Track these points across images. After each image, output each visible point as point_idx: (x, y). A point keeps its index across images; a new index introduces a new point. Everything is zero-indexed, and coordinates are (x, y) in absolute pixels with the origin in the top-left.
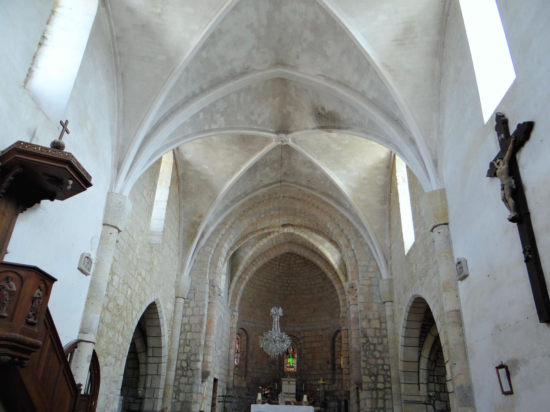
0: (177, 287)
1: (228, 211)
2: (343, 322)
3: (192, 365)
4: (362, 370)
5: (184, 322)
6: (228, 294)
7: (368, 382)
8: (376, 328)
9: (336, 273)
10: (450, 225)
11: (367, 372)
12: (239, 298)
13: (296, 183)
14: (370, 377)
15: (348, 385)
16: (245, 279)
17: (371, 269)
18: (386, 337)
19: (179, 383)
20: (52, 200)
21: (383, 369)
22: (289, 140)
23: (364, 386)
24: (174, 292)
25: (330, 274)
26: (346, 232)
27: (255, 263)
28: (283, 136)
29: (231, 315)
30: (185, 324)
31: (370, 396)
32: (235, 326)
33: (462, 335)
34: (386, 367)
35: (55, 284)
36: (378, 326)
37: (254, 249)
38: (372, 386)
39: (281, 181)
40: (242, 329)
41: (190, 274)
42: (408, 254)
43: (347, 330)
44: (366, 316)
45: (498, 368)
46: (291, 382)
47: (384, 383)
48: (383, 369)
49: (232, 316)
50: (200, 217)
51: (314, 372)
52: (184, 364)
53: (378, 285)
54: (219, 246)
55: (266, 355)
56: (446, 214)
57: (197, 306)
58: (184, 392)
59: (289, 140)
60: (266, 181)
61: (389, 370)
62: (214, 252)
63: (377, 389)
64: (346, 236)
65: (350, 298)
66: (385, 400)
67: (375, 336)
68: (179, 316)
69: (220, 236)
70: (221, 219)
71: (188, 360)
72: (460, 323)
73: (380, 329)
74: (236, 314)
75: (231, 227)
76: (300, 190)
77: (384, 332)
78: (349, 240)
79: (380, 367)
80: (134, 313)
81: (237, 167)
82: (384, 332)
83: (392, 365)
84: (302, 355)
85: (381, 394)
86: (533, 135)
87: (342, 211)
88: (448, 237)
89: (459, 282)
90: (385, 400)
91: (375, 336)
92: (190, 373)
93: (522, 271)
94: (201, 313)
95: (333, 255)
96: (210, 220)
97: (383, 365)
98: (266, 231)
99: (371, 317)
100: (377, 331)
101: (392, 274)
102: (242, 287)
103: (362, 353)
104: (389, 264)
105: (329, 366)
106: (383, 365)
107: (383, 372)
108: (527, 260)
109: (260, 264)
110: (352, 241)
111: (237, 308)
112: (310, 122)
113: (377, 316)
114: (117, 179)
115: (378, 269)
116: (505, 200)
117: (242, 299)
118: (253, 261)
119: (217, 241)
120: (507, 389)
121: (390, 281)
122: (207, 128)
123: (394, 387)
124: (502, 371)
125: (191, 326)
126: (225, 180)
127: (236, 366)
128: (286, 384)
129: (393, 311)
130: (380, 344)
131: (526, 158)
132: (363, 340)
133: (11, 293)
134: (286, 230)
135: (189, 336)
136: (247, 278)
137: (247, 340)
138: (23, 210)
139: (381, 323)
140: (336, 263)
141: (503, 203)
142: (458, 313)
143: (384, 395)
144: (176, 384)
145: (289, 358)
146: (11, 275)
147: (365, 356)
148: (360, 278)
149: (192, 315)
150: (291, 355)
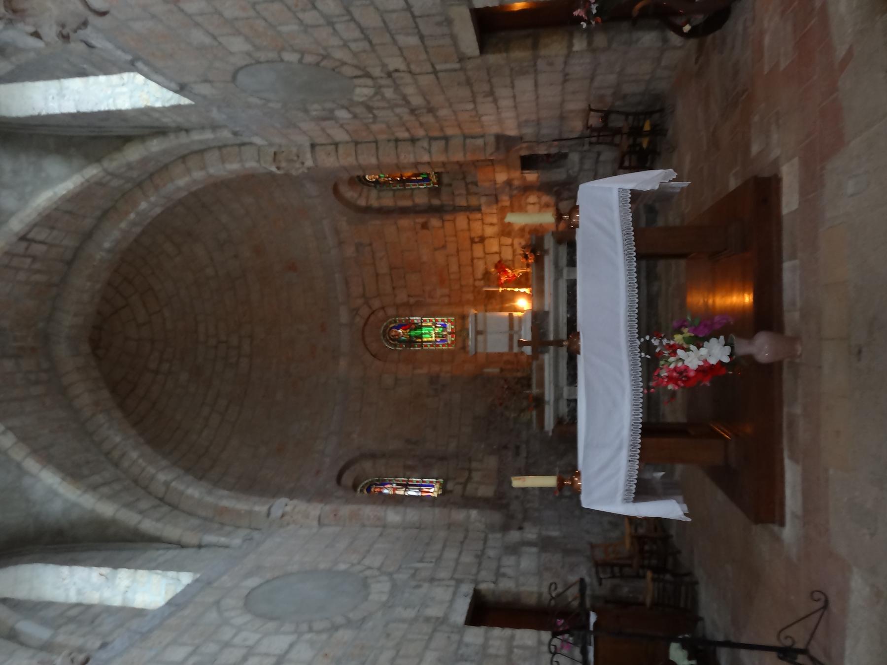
2: (290, 161)
6: (200, 546)
15: (480, 142)
16: (167, 484)
25: (143, 205)
27: (116, 454)
29: (281, 526)
37: (31, 465)
43: (313, 146)
46: (480, 328)
51: (454, 268)
55: (796, 211)
74: (281, 505)
84: (412, 300)
95: (48, 182)
105: (435, 222)
128: (485, 341)
137: (373, 456)
145: (420, 337)
150: (413, 333)
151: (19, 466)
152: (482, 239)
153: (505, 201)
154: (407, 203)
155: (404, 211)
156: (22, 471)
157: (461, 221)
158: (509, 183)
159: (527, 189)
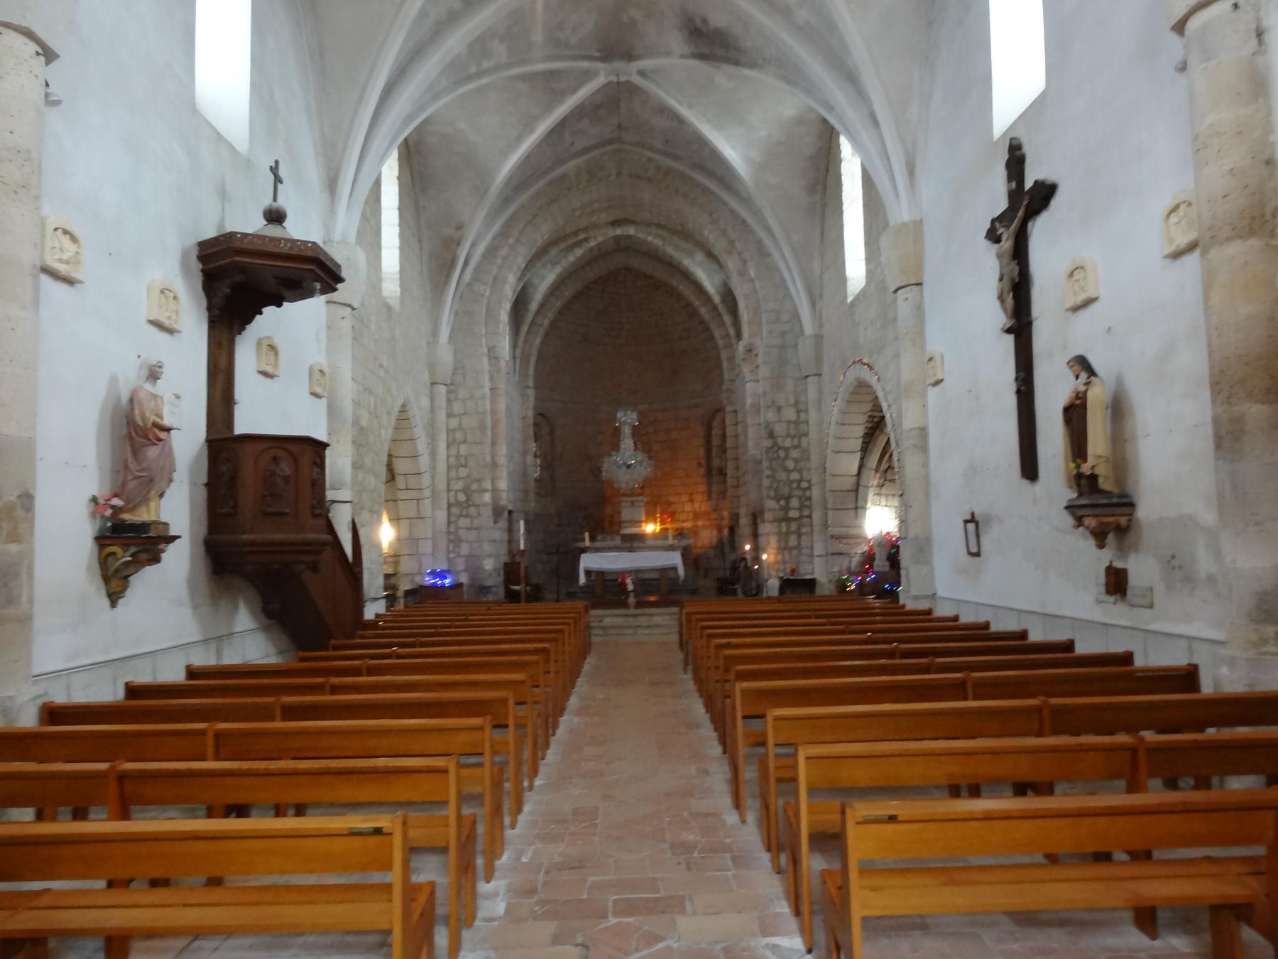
0: (432, 367)
1: (511, 209)
3: (476, 498)
4: (765, 491)
5: (452, 427)
7: (774, 510)
8: (789, 422)
9: (715, 308)
10: (927, 289)
11: (772, 493)
12: (533, 361)
13: (640, 144)
14: (778, 501)
16: (541, 325)
17: (785, 317)
18: (806, 435)
19: (458, 528)
20: (279, 305)
21: (799, 487)
22: (630, 72)
23: (768, 516)
24: (426, 376)
26: (739, 246)
28: (618, 65)
30: (454, 430)
31: (776, 530)
32: (530, 413)
33: (925, 465)
34: (804, 485)
35: (328, 452)
36: (793, 418)
37: (558, 269)
38: (781, 514)
39: (610, 142)
40: (541, 414)
41: (450, 338)
42: (853, 303)
44: (773, 402)
45: (966, 522)
47: (800, 509)
48: (799, 487)
49: (524, 396)
50: (460, 227)
52: (462, 497)
53: (796, 346)
54: (497, 281)
56: (919, 267)
57: (472, 397)
58: (466, 541)
59: (630, 72)
60: (581, 144)
61: (809, 488)
62: (491, 293)
63: (788, 520)
64: (740, 254)
65: (746, 369)
66: (800, 535)
67: (788, 435)
68: (441, 416)
69: (499, 261)
70: (497, 227)
71: (466, 491)
72: (924, 448)
73: (797, 423)
74: (531, 393)
75: (517, 241)
76: (650, 160)
77: (803, 427)
78: (744, 262)
79: (795, 485)
80: (383, 432)
81: (528, 127)
82: (803, 427)
83: (814, 481)
85: (794, 527)
86: (1054, 203)
87: (733, 204)
88: (919, 309)
89: (930, 388)
90: (800, 535)
91: (788, 435)
92: (472, 511)
93: (1011, 401)
94: (481, 410)
96: (478, 232)
97: (799, 481)
98: (581, 236)
99: (782, 402)
100: (792, 426)
101: (821, 326)
102: (538, 341)
103: (765, 464)
104: (818, 307)
105: (702, 471)
106: (799, 481)
107: (797, 493)
108: (1018, 392)
109: (568, 293)
110: (750, 264)
111: (531, 382)
112: (677, 42)
113: (792, 401)
114: (332, 212)
115: (796, 316)
116: (1001, 298)
117: (538, 360)
118: (555, 289)
119: (494, 272)
120: (974, 549)
121: (818, 338)
122: (473, 69)
123: (816, 516)
124: (971, 526)
125: (465, 434)
126: (505, 154)
127: (536, 480)
129: (820, 392)
130: (796, 447)
131: (1040, 229)
132: (768, 443)
133: (286, 480)
134: (619, 231)
135: (463, 449)
136: (546, 322)
137: (552, 433)
138: (242, 329)
139: (798, 412)
140: (718, 292)
141: (997, 303)
142: (923, 431)
143: (799, 528)
144: (452, 529)
146: (280, 453)
147: (771, 468)
148: (765, 334)
149: (465, 414)
151: (558, 263)
152: (691, 501)
153: (714, 516)
154: (714, 454)
155: (709, 451)
156: (554, 264)
157: (702, 488)
158: (723, 519)
159: (720, 529)
